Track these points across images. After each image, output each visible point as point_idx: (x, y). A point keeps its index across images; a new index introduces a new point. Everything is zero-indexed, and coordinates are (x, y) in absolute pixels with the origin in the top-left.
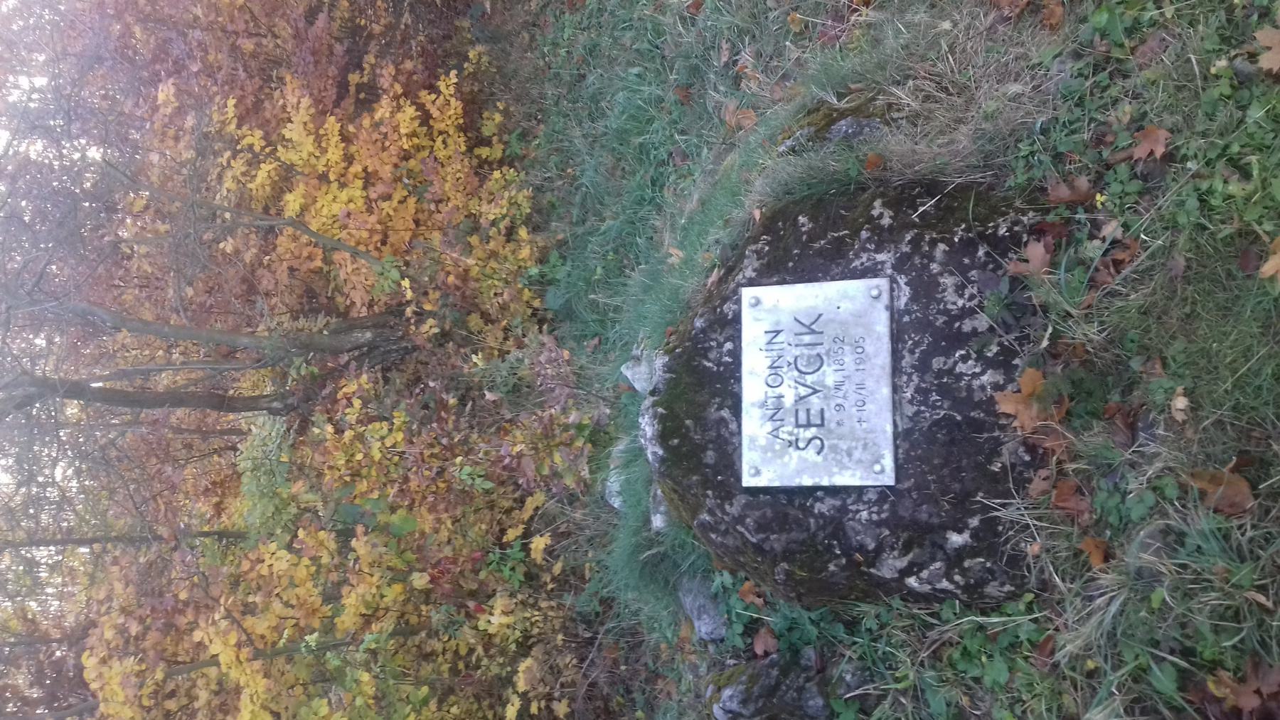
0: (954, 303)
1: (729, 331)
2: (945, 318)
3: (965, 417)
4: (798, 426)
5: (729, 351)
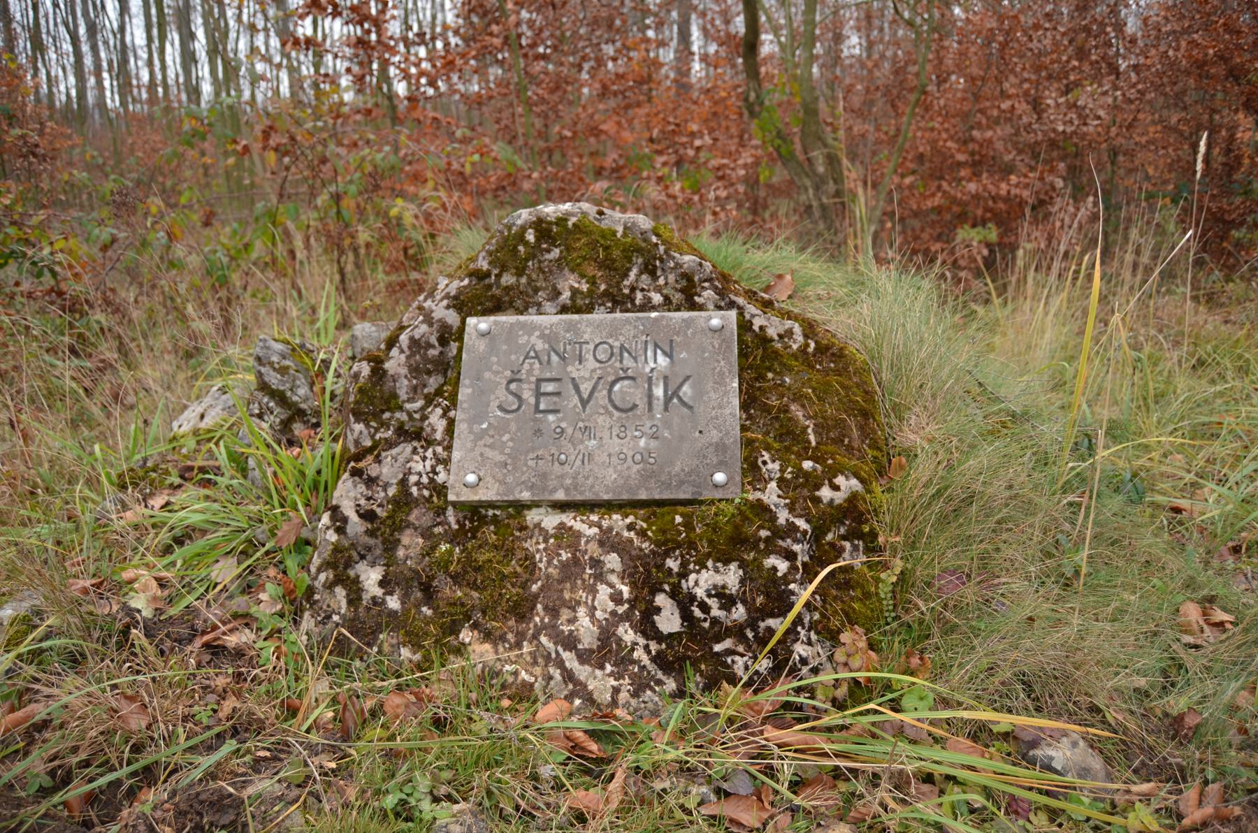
0: (696, 583)
1: (677, 297)
2: (676, 570)
3: (536, 596)
4: (539, 381)
5: (650, 300)
